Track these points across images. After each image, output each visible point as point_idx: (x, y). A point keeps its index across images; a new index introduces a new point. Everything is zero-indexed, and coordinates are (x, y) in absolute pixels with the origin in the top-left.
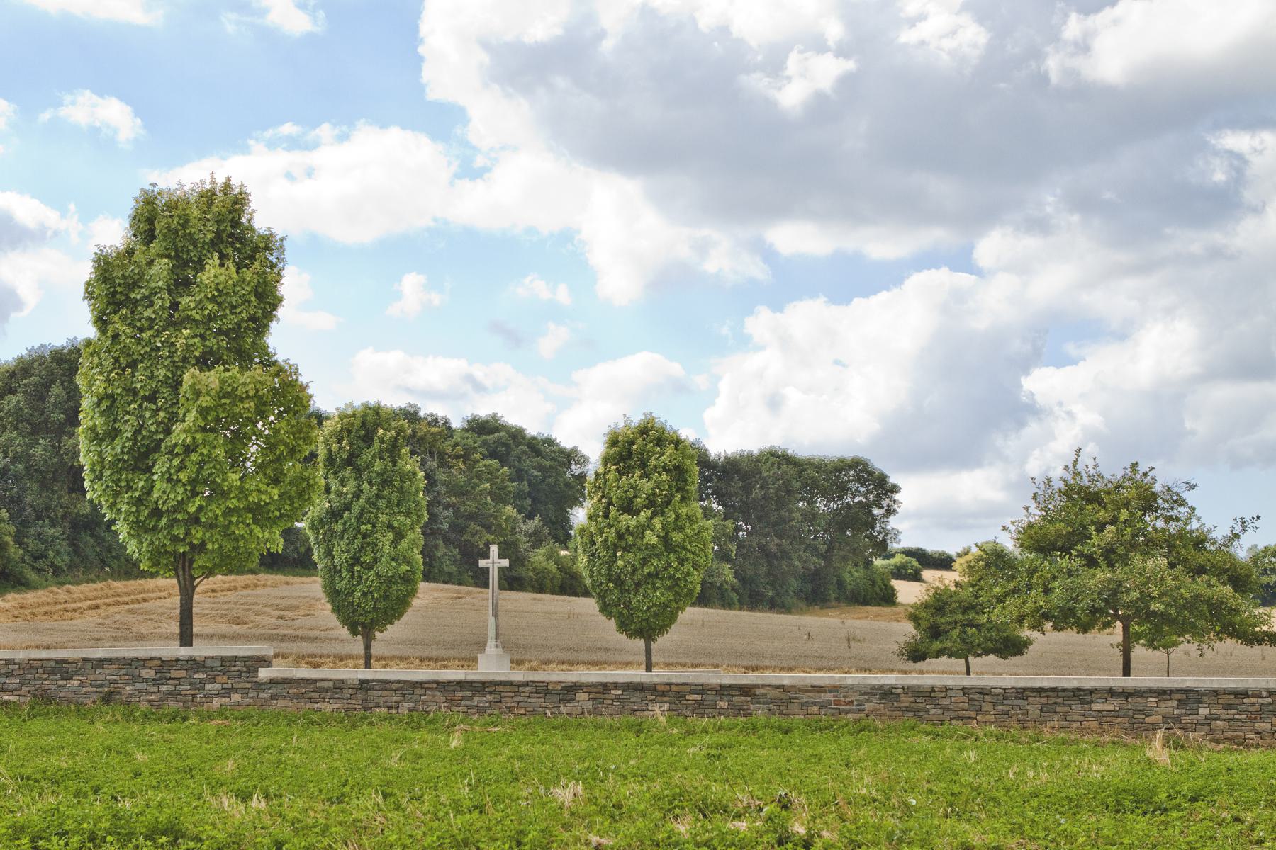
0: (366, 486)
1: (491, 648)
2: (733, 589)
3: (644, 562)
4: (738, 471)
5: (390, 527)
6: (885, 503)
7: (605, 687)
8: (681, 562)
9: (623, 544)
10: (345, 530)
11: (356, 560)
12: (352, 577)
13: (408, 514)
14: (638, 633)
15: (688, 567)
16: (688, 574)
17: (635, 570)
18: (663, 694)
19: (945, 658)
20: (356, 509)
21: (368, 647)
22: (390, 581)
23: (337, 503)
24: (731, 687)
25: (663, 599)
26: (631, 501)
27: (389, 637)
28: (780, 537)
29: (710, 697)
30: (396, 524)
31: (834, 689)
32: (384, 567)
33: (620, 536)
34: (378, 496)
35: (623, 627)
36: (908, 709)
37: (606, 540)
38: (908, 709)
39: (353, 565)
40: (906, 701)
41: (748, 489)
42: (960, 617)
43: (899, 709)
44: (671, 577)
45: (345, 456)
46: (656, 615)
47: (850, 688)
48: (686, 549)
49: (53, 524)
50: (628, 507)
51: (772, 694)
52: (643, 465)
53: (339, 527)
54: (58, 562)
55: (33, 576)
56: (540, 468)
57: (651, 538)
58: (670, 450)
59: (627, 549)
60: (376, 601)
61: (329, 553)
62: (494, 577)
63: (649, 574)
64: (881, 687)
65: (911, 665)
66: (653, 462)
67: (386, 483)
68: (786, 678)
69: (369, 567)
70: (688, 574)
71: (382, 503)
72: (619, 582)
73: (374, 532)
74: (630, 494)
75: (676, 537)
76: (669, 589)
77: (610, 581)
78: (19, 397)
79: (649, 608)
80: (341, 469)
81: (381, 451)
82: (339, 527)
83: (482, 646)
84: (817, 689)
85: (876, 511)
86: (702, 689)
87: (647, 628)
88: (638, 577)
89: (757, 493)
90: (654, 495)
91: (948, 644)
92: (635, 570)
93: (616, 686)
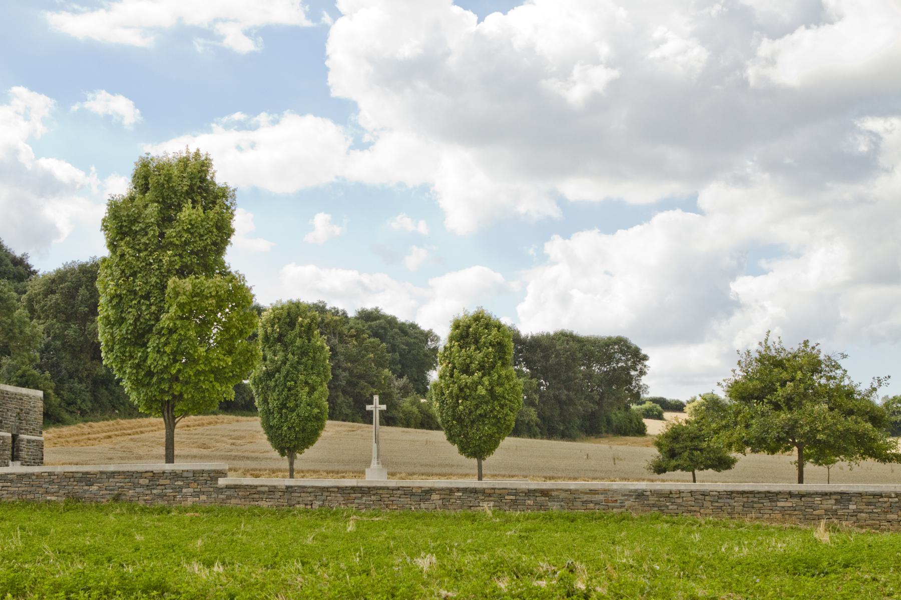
0: (290, 356)
1: (374, 464)
2: (537, 425)
3: (477, 407)
4: (540, 346)
5: (307, 383)
6: (639, 367)
7: (451, 491)
8: (502, 407)
9: (463, 395)
10: (276, 385)
11: (284, 406)
12: (281, 417)
13: (318, 375)
14: (474, 454)
15: (506, 410)
16: (507, 415)
17: (471, 412)
18: (490, 495)
19: (679, 472)
20: (284, 371)
21: (291, 464)
22: (307, 419)
23: (271, 368)
24: (535, 491)
25: (490, 432)
26: (468, 366)
27: (307, 457)
28: (569, 390)
29: (521, 497)
30: (310, 381)
31: (605, 492)
32: (303, 410)
33: (461, 390)
34: (299, 363)
35: (463, 450)
36: (654, 506)
37: (451, 392)
38: (654, 506)
39: (281, 409)
40: (652, 500)
41: (546, 358)
42: (689, 444)
43: (648, 505)
44: (495, 417)
45: (276, 336)
46: (485, 442)
47: (615, 491)
48: (505, 398)
49: (81, 381)
50: (466, 370)
51: (563, 495)
52: (476, 342)
53: (272, 384)
54: (83, 407)
55: (66, 416)
56: (407, 344)
57: (481, 391)
58: (494, 331)
59: (465, 398)
60: (297, 433)
61: (265, 401)
62: (376, 417)
63: (480, 415)
64: (636, 491)
65: (656, 476)
66: (483, 340)
67: (304, 353)
68: (572, 485)
69: (293, 410)
70: (507, 415)
71: (301, 367)
72: (460, 420)
73: (295, 387)
74: (468, 361)
75: (499, 390)
76: (494, 425)
77: (454, 419)
78: (57, 296)
79: (480, 438)
80: (274, 344)
81: (300, 332)
82: (272, 384)
83: (368, 463)
84: (593, 492)
85: (633, 373)
86: (516, 492)
87: (478, 449)
88: (473, 417)
89: (552, 360)
90: (483, 361)
91: (681, 462)
92: (471, 412)
93: (458, 490)
